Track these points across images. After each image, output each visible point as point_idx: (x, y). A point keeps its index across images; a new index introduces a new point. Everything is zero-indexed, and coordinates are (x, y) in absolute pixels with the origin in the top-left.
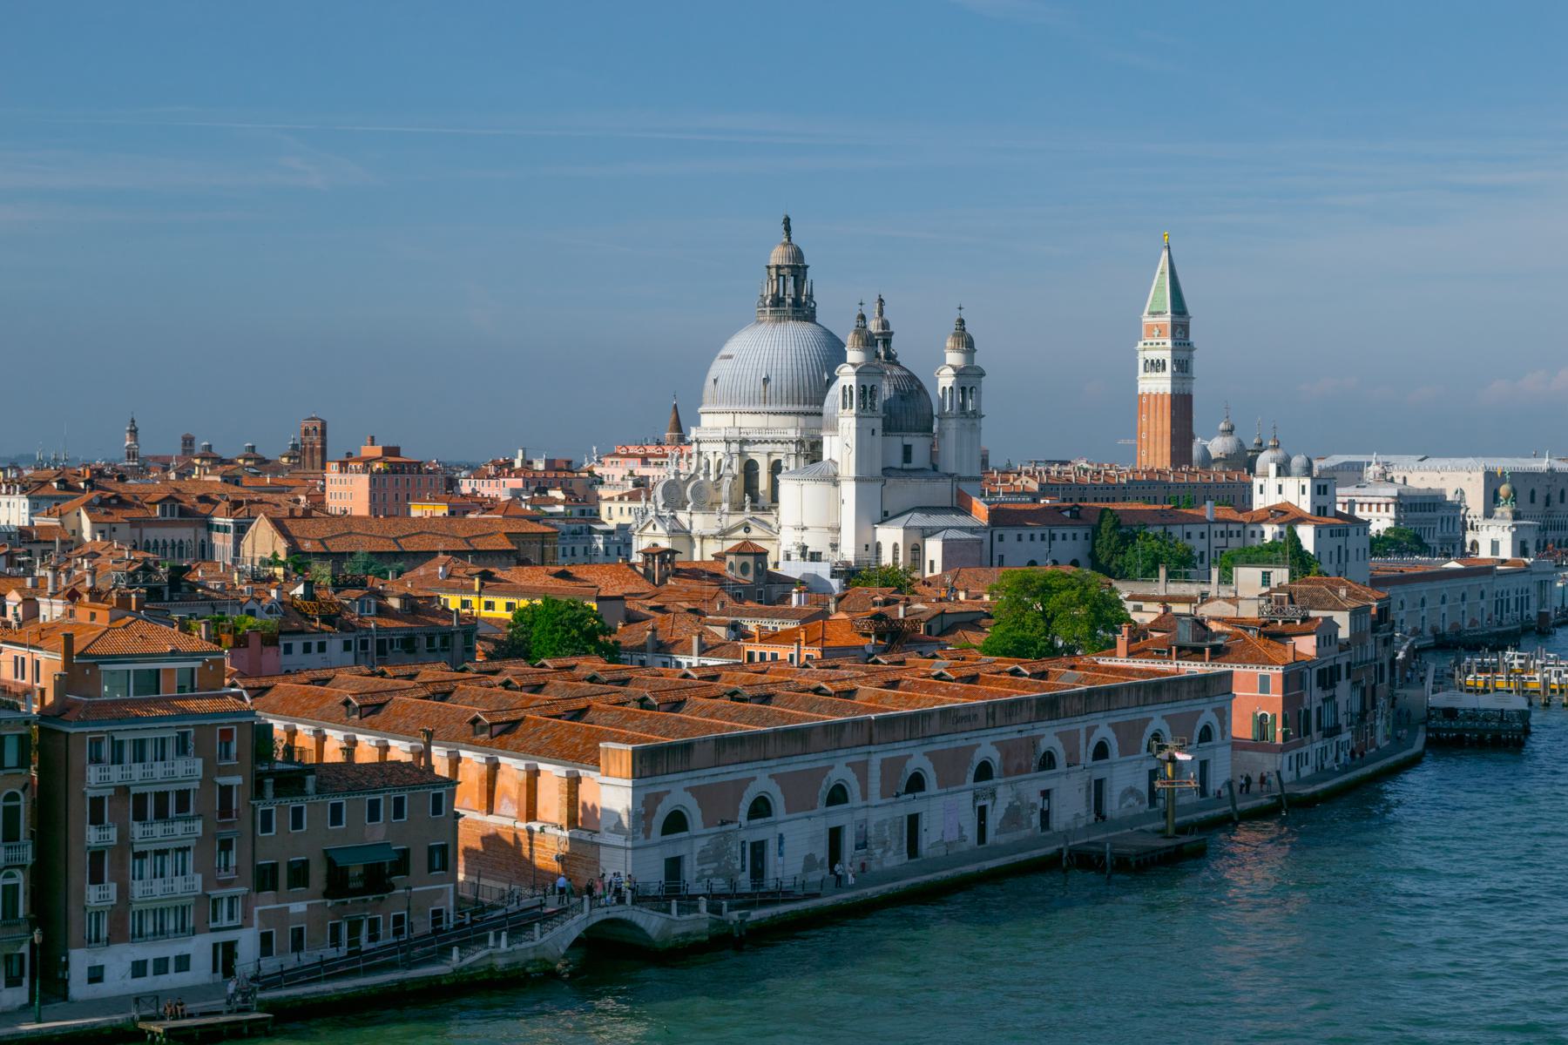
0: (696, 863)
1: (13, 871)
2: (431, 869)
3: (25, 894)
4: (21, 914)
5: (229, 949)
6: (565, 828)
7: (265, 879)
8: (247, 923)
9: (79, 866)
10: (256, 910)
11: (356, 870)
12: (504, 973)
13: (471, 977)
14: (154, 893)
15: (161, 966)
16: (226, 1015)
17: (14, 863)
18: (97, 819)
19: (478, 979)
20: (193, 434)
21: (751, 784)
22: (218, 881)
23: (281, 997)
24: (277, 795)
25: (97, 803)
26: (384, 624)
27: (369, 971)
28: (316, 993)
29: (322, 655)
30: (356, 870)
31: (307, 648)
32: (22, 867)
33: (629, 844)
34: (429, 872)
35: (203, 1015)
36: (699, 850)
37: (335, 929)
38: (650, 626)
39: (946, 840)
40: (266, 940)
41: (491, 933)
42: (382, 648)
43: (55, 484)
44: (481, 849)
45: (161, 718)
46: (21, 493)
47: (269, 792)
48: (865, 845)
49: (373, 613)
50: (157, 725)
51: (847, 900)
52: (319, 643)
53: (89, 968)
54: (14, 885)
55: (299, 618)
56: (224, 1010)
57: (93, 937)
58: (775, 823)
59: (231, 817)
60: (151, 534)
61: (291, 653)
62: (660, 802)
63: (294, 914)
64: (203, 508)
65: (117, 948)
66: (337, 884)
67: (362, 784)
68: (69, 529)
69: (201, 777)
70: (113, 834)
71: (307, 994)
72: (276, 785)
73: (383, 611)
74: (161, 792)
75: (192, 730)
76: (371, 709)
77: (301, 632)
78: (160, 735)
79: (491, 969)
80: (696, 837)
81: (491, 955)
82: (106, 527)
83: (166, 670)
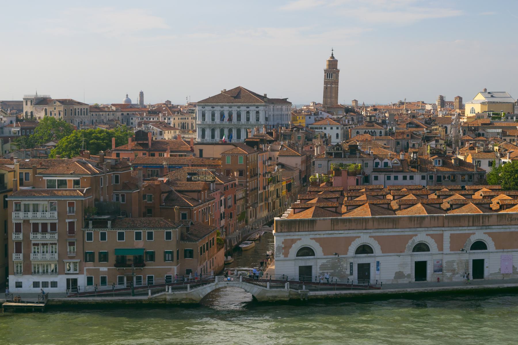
0: (318, 269)
2: (165, 260)
5: (75, 281)
7: (89, 257)
8: (81, 272)
9: (12, 247)
10: (85, 268)
11: (130, 257)
12: (170, 302)
13: (155, 302)
14: (38, 258)
15: (45, 284)
19: (159, 303)
20: (439, 95)
21: (357, 239)
26: (442, 170)
27: (116, 295)
30: (130, 257)
31: (405, 178)
34: (164, 261)
36: (321, 264)
39: (501, 273)
40: (90, 281)
42: (439, 179)
47: (91, 226)
48: (441, 270)
50: (41, 199)
51: (392, 292)
58: (375, 256)
61: (397, 179)
62: (294, 243)
66: (121, 262)
69: (57, 218)
71: (81, 300)
72: (93, 224)
74: (18, 223)
79: (165, 300)
80: (319, 258)
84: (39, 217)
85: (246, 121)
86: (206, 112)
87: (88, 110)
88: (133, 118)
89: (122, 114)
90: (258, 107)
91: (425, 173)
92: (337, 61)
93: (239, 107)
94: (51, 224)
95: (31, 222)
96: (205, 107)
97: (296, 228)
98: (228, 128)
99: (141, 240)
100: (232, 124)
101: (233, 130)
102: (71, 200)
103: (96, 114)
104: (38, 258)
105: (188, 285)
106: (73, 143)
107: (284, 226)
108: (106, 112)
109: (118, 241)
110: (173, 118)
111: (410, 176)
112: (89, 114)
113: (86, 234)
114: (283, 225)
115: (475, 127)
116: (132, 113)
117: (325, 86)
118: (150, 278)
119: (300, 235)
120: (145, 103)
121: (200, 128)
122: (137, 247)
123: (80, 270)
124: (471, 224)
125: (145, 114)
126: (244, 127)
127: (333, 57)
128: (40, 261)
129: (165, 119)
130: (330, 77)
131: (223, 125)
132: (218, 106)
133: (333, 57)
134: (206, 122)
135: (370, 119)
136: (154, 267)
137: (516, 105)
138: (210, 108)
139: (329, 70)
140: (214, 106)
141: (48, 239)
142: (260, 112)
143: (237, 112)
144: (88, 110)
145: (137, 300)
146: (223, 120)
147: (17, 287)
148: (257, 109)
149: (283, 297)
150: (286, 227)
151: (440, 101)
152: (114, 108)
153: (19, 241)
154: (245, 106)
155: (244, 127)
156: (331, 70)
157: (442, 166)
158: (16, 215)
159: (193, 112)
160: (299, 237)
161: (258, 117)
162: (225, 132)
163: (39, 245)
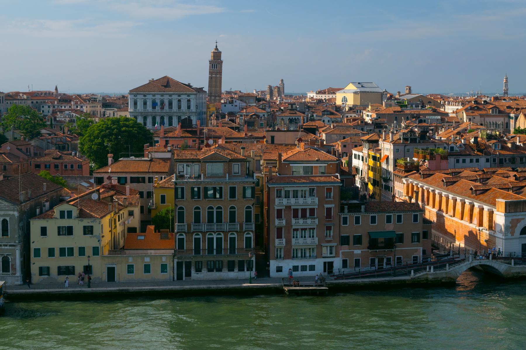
1: (182, 233)
2: (412, 242)
3: (253, 240)
4: (252, 247)
5: (331, 264)
6: (488, 230)
7: (344, 241)
8: (337, 255)
9: (274, 233)
10: (341, 251)
11: (381, 239)
14: (300, 243)
15: (304, 268)
16: (314, 287)
17: (249, 230)
18: (279, 216)
22: (326, 241)
23: (340, 282)
24: (349, 211)
25: (279, 212)
26: (503, 153)
28: (354, 282)
29: (477, 163)
30: (381, 239)
31: (471, 161)
32: (252, 231)
33: (504, 237)
35: (306, 286)
37: (373, 261)
38: (86, 152)
40: (345, 263)
41: (428, 267)
43: (473, 102)
44: (468, 236)
45: (304, 183)
46: (461, 105)
47: (346, 210)
49: (500, 148)
50: (302, 185)
52: (476, 159)
53: (277, 267)
54: (250, 237)
55: (470, 149)
56: (314, 285)
57: (295, 256)
59: (331, 218)
60: (488, 120)
62: (519, 222)
63: (356, 254)
64: (508, 111)
65: (287, 261)
66: (373, 244)
67: (385, 209)
68: (459, 117)
69: (317, 204)
70: (284, 222)
71: (350, 282)
72: (348, 209)
73: (504, 148)
75: (316, 188)
76: (451, 183)
77: (469, 155)
78: (304, 189)
79: (427, 279)
81: (427, 274)
82: (471, 117)
83: (315, 167)
84: (299, 203)
85: (177, 109)
86: (138, 100)
87: (4, 98)
88: (45, 106)
89: (32, 102)
90: (190, 96)
91: (489, 156)
92: (221, 52)
93: (171, 95)
94: (302, 209)
95: (292, 207)
96: (137, 96)
97: (521, 208)
98: (160, 115)
99: (391, 223)
100: (164, 112)
101: (165, 118)
102: (330, 186)
103: (11, 102)
104: (300, 243)
105: (428, 266)
106: (106, 131)
108: (19, 100)
109: (370, 224)
110: (86, 106)
111: (476, 159)
112: (4, 102)
113: (342, 219)
114: (511, 206)
115: (417, 115)
116: (40, 101)
117: (210, 76)
118: (399, 259)
119: (524, 215)
120: (59, 92)
121: (132, 115)
122: (387, 230)
123: (336, 254)
125: (56, 102)
126: (176, 114)
127: (217, 49)
128: (309, 245)
129: (77, 107)
130: (214, 68)
131: (155, 113)
132: (150, 94)
133: (217, 49)
134: (138, 110)
135: (292, 107)
136: (400, 249)
137: (384, 94)
138: (142, 96)
139: (214, 61)
140: (146, 95)
141: (309, 224)
142: (192, 100)
143: (169, 100)
144: (4, 98)
145: (401, 280)
146: (172, 108)
147: (277, 271)
148: (188, 98)
151: (269, 90)
152: (25, 97)
153: (280, 227)
154: (176, 94)
155: (176, 114)
156: (215, 61)
157: (501, 150)
158: (280, 201)
159: (95, 100)
160: (523, 217)
161: (189, 105)
162: (157, 119)
163: (298, 231)
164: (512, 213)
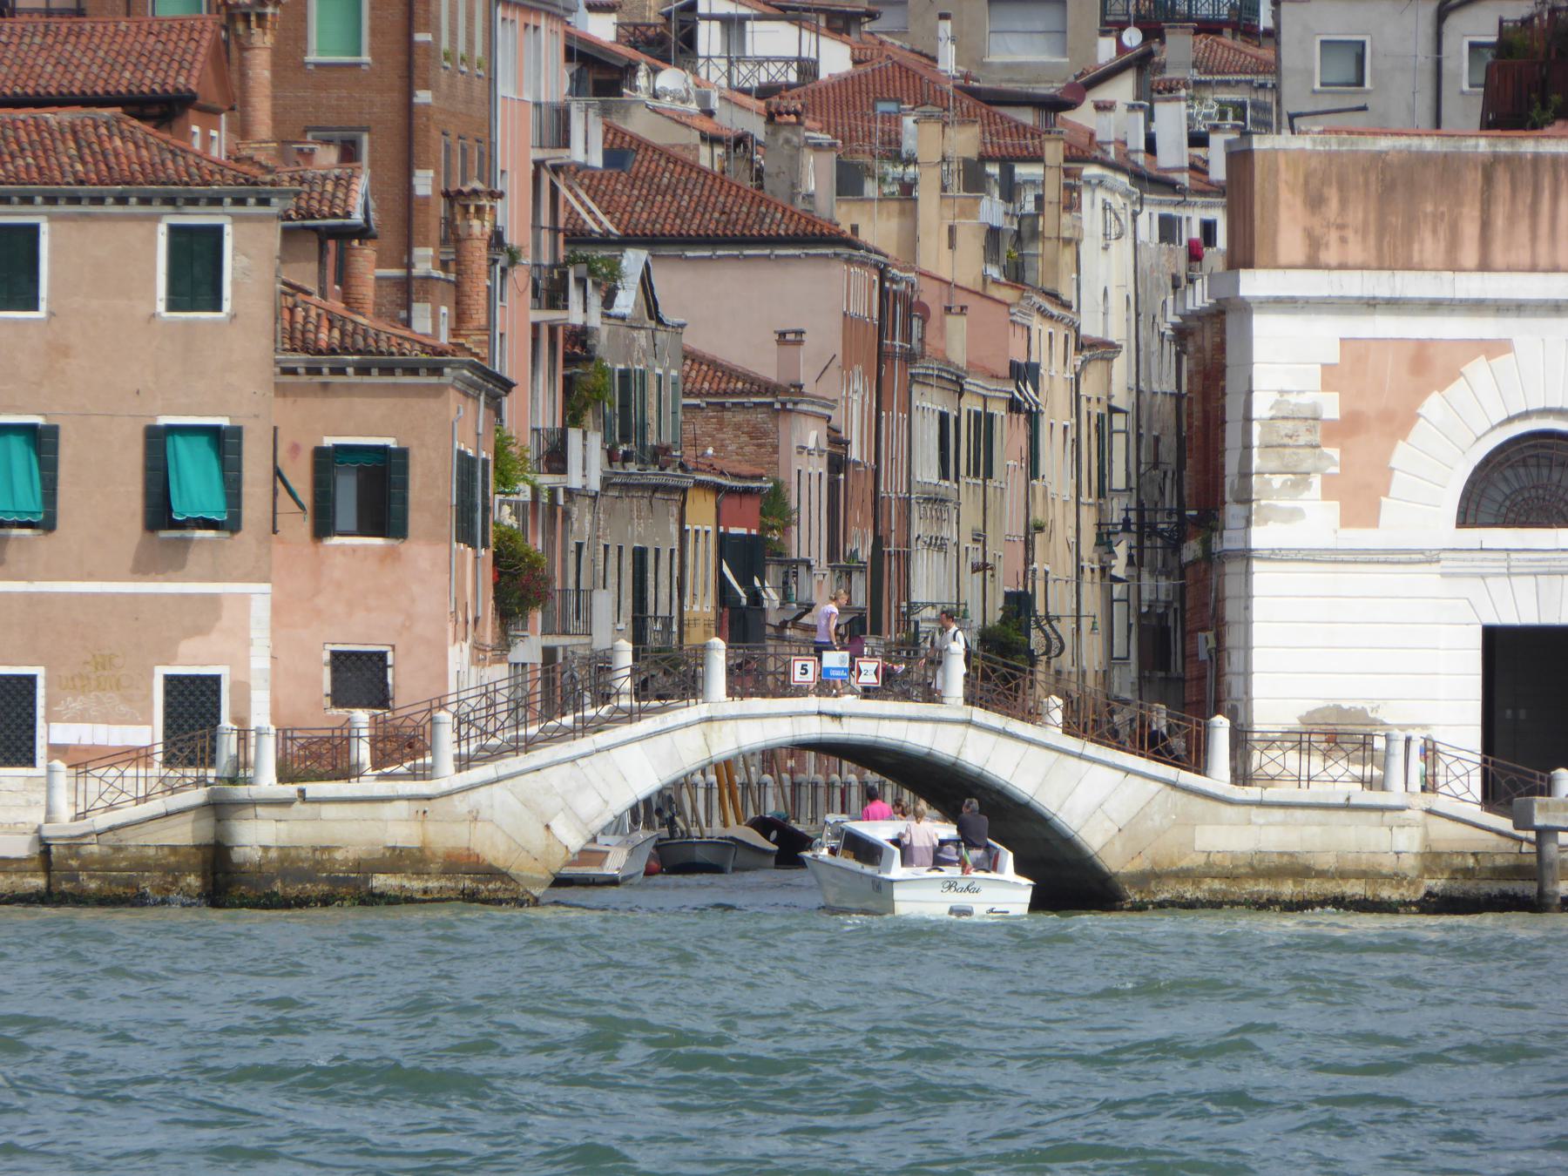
62: (1441, 387)
107: (1344, 203)
124: (1470, 254)
149: (1362, 875)
150: (1356, 215)
164: (1343, 267)
